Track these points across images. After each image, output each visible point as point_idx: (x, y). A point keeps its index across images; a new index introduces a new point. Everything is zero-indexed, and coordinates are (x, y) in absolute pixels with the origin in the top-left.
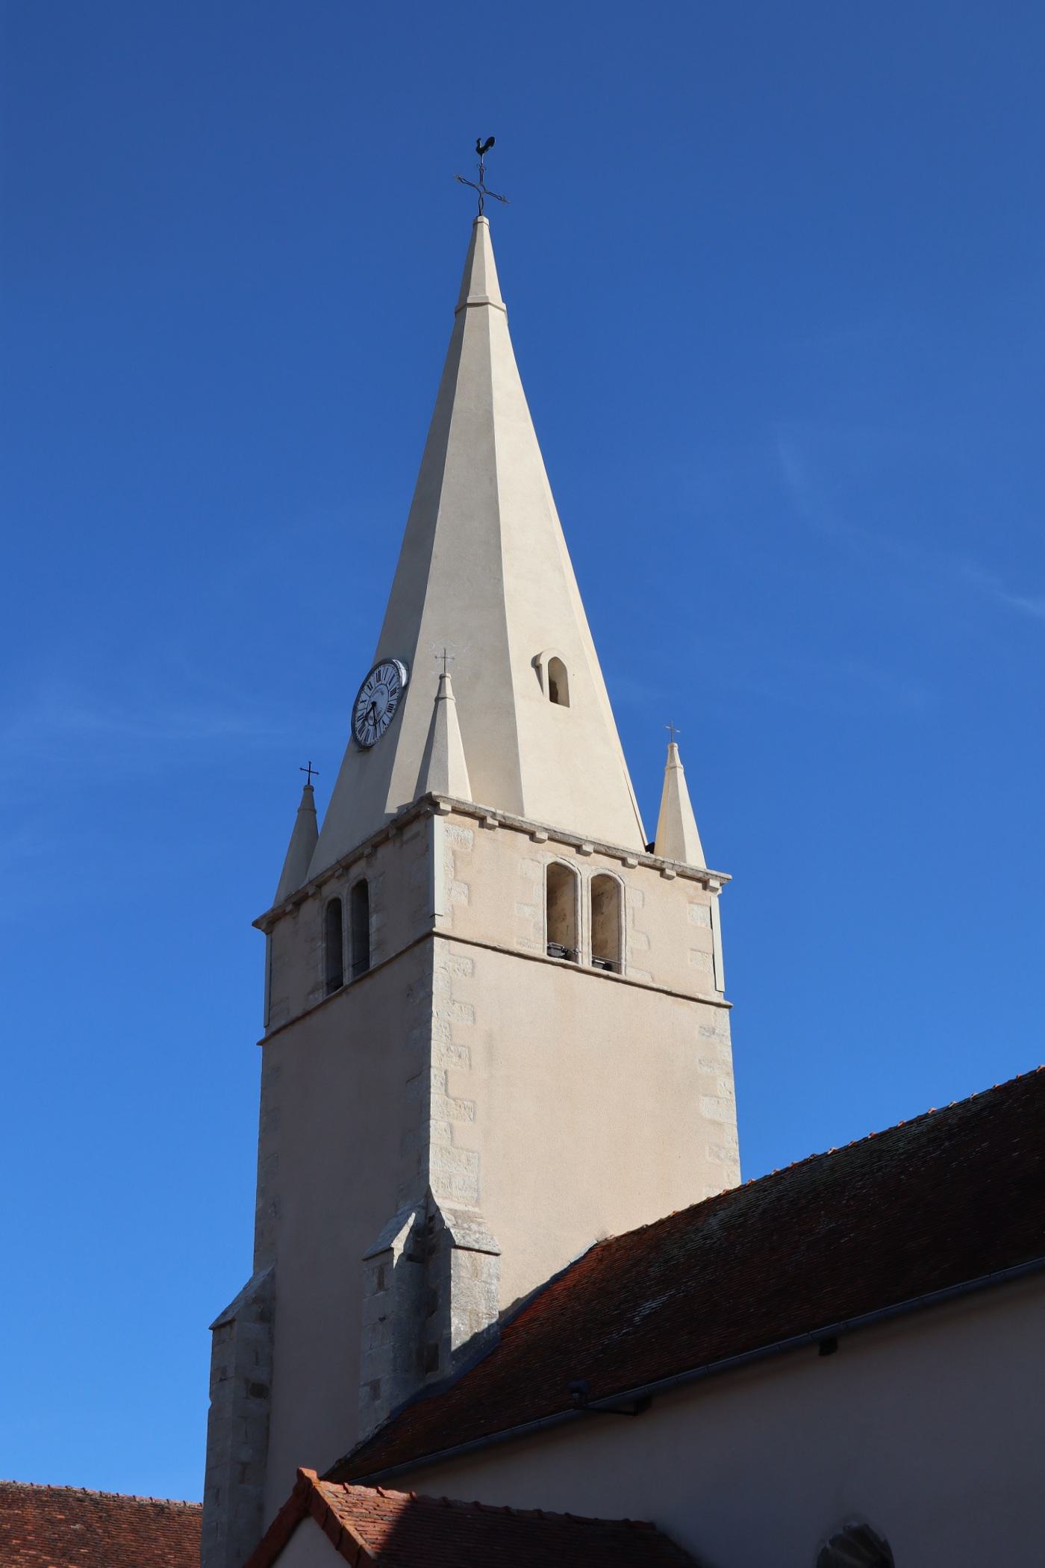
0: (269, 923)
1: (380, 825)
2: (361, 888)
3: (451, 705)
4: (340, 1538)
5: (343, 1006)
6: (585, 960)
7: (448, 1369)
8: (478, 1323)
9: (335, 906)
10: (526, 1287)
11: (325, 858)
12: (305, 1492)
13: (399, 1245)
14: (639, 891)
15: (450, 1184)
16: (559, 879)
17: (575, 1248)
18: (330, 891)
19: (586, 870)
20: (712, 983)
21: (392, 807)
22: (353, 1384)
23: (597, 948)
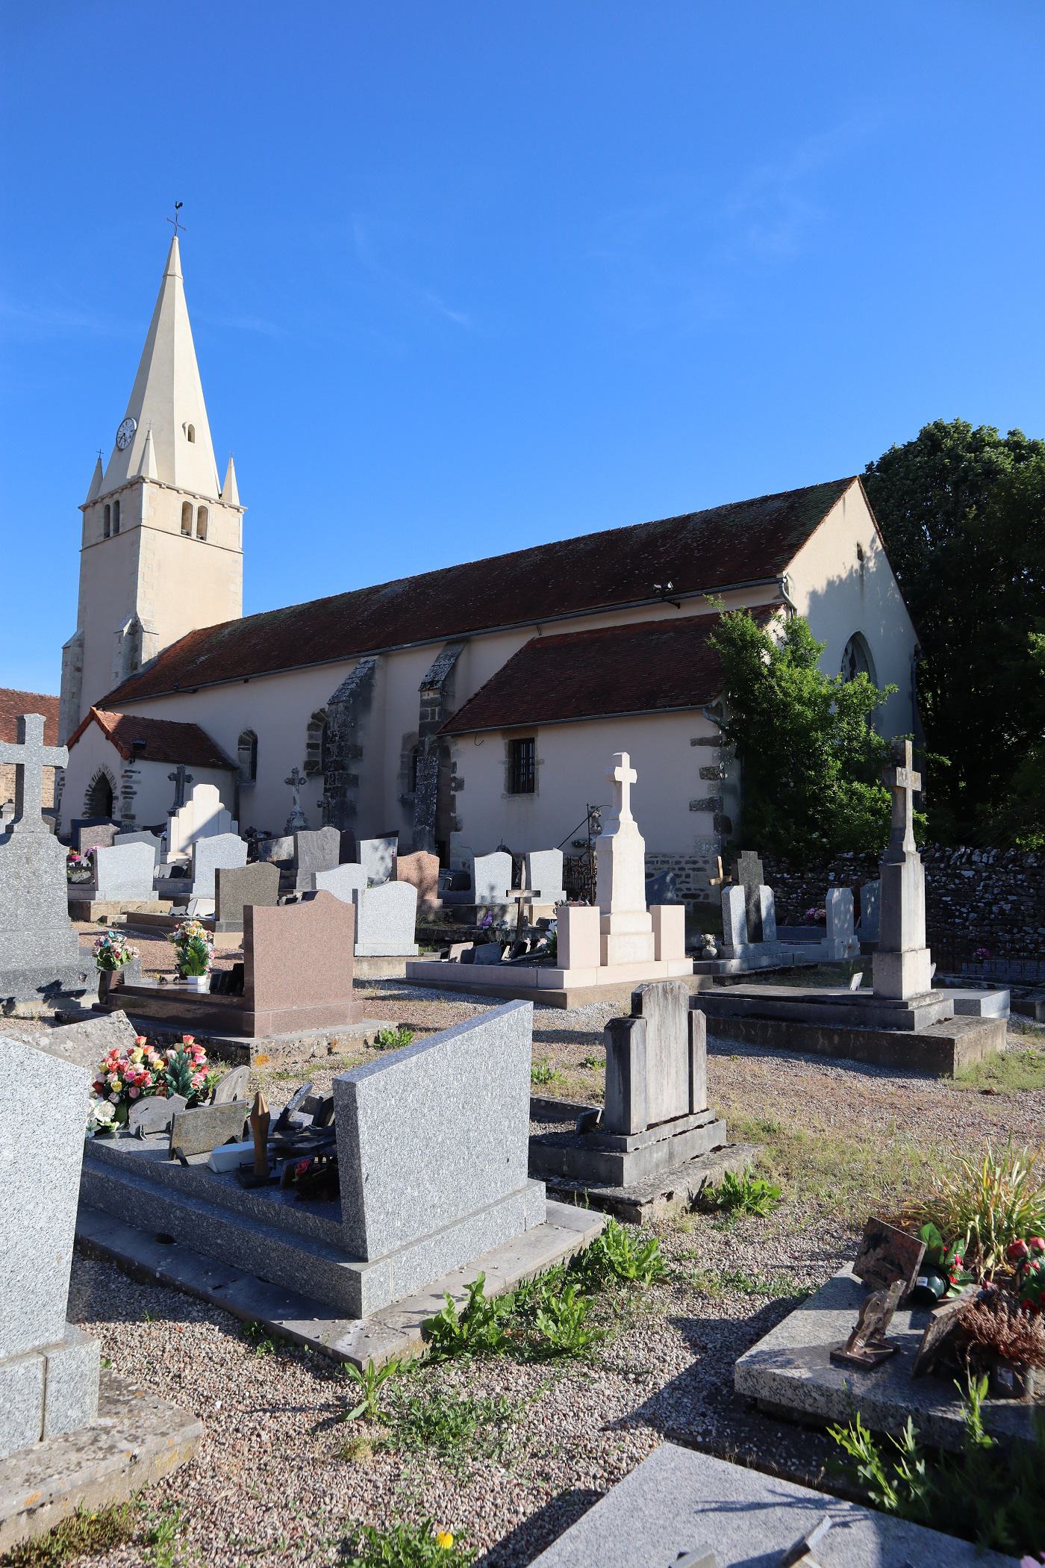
0: (84, 508)
1: (122, 483)
2: (117, 503)
3: (151, 442)
4: (103, 727)
5: (110, 544)
6: (194, 535)
7: (140, 670)
8: (335, 1339)
9: (108, 507)
10: (168, 645)
11: (105, 490)
12: (93, 713)
13: (126, 630)
14: (214, 512)
15: (144, 610)
16: (186, 507)
17: (183, 632)
18: (107, 501)
19: (196, 504)
20: (237, 544)
21: (129, 476)
22: (108, 677)
23: (198, 532)
